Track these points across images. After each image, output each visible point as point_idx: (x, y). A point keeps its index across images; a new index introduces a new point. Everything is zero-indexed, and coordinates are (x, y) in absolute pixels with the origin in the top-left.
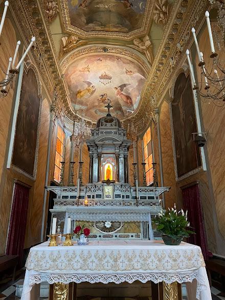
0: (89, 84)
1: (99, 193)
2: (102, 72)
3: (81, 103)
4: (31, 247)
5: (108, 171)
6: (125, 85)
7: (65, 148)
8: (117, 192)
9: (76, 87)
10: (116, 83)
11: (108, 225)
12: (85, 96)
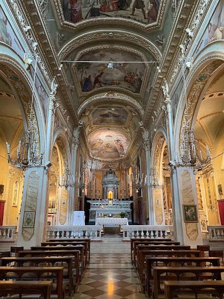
0: (100, 140)
1: (107, 203)
2: (107, 134)
3: (96, 149)
4: (223, 35)
5: (110, 194)
6: (119, 140)
7: (139, 217)
8: (114, 203)
9: (93, 142)
10: (115, 139)
11: (110, 215)
12: (98, 146)
